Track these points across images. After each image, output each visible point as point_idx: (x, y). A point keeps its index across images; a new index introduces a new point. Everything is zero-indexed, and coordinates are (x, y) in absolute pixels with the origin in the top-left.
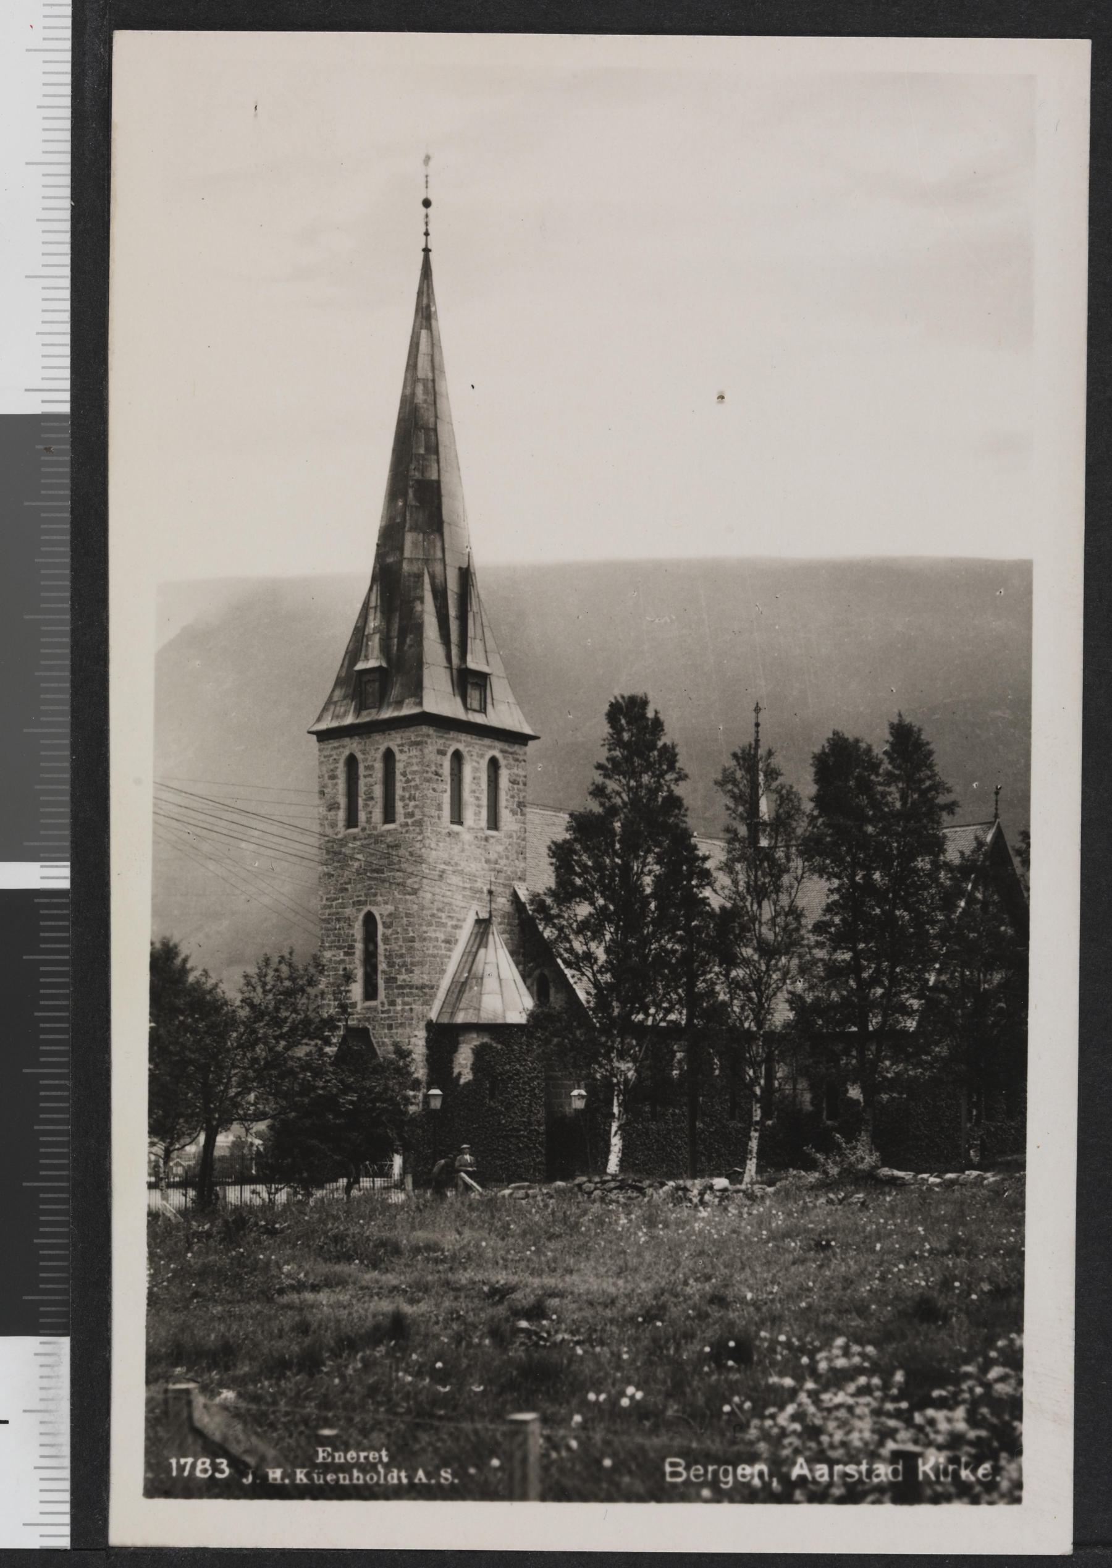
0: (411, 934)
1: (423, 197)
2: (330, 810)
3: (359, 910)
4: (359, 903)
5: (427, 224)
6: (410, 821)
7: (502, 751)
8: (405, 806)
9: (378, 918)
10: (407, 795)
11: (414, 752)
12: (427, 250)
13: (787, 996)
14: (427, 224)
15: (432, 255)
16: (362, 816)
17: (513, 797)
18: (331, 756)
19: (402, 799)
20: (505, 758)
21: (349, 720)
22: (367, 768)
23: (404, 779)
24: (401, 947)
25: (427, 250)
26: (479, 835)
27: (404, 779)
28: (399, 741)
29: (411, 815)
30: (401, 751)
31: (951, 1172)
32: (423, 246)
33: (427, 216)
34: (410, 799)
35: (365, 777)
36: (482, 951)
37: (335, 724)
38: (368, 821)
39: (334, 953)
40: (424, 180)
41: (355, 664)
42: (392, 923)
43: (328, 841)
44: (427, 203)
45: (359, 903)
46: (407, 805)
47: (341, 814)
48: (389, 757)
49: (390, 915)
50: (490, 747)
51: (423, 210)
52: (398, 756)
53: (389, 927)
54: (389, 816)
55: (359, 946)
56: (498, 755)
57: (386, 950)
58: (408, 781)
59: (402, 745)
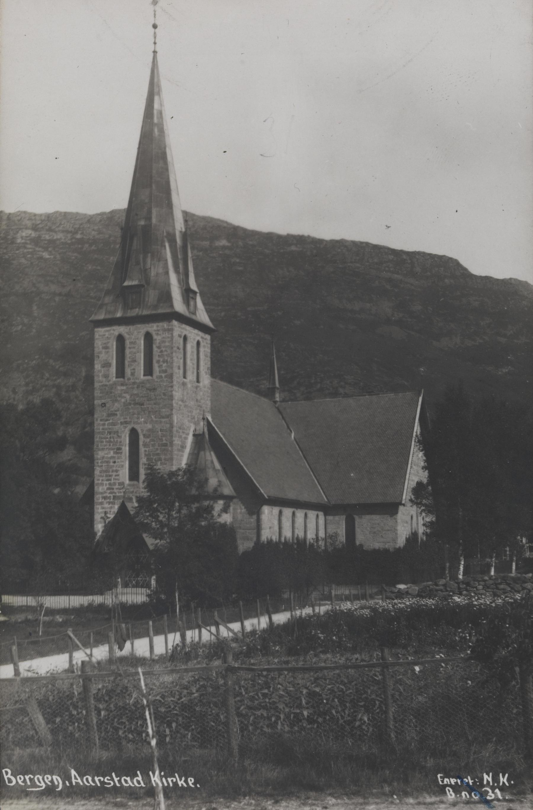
0: (164, 442)
1: (153, 22)
2: (103, 367)
3: (125, 427)
4: (126, 423)
5: (155, 38)
6: (163, 375)
7: (202, 338)
8: (160, 366)
9: (139, 431)
10: (161, 360)
11: (167, 335)
12: (155, 52)
13: (148, 538)
14: (155, 38)
15: (158, 55)
16: (128, 371)
17: (206, 364)
18: (104, 335)
19: (158, 362)
20: (203, 341)
21: (119, 315)
22: (131, 343)
23: (159, 350)
24: (157, 449)
25: (155, 52)
26: (194, 385)
27: (159, 350)
28: (155, 328)
29: (165, 371)
30: (157, 334)
31: (145, 713)
32: (153, 50)
33: (155, 33)
34: (164, 362)
35: (130, 348)
36: (202, 453)
37: (109, 316)
38: (133, 374)
39: (106, 452)
40: (153, 13)
41: (124, 283)
42: (150, 435)
43: (102, 386)
44: (155, 26)
45: (126, 423)
46: (162, 365)
47: (113, 370)
48: (148, 337)
49: (149, 430)
50: (197, 335)
51: (153, 30)
52: (155, 337)
53: (148, 437)
54: (149, 370)
55: (126, 449)
56: (201, 340)
57: (145, 451)
58: (161, 352)
59: (158, 330)
